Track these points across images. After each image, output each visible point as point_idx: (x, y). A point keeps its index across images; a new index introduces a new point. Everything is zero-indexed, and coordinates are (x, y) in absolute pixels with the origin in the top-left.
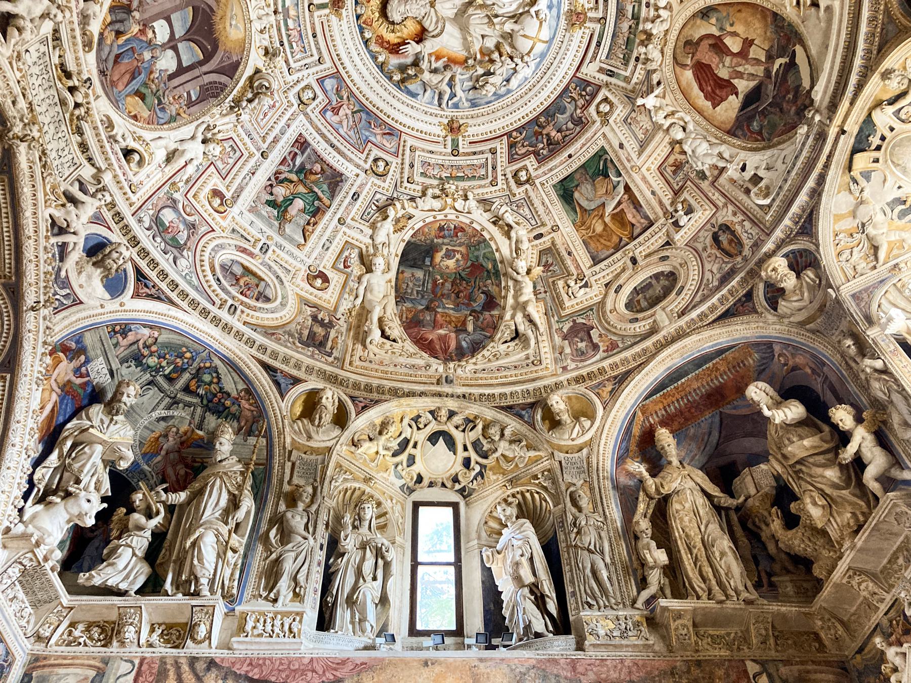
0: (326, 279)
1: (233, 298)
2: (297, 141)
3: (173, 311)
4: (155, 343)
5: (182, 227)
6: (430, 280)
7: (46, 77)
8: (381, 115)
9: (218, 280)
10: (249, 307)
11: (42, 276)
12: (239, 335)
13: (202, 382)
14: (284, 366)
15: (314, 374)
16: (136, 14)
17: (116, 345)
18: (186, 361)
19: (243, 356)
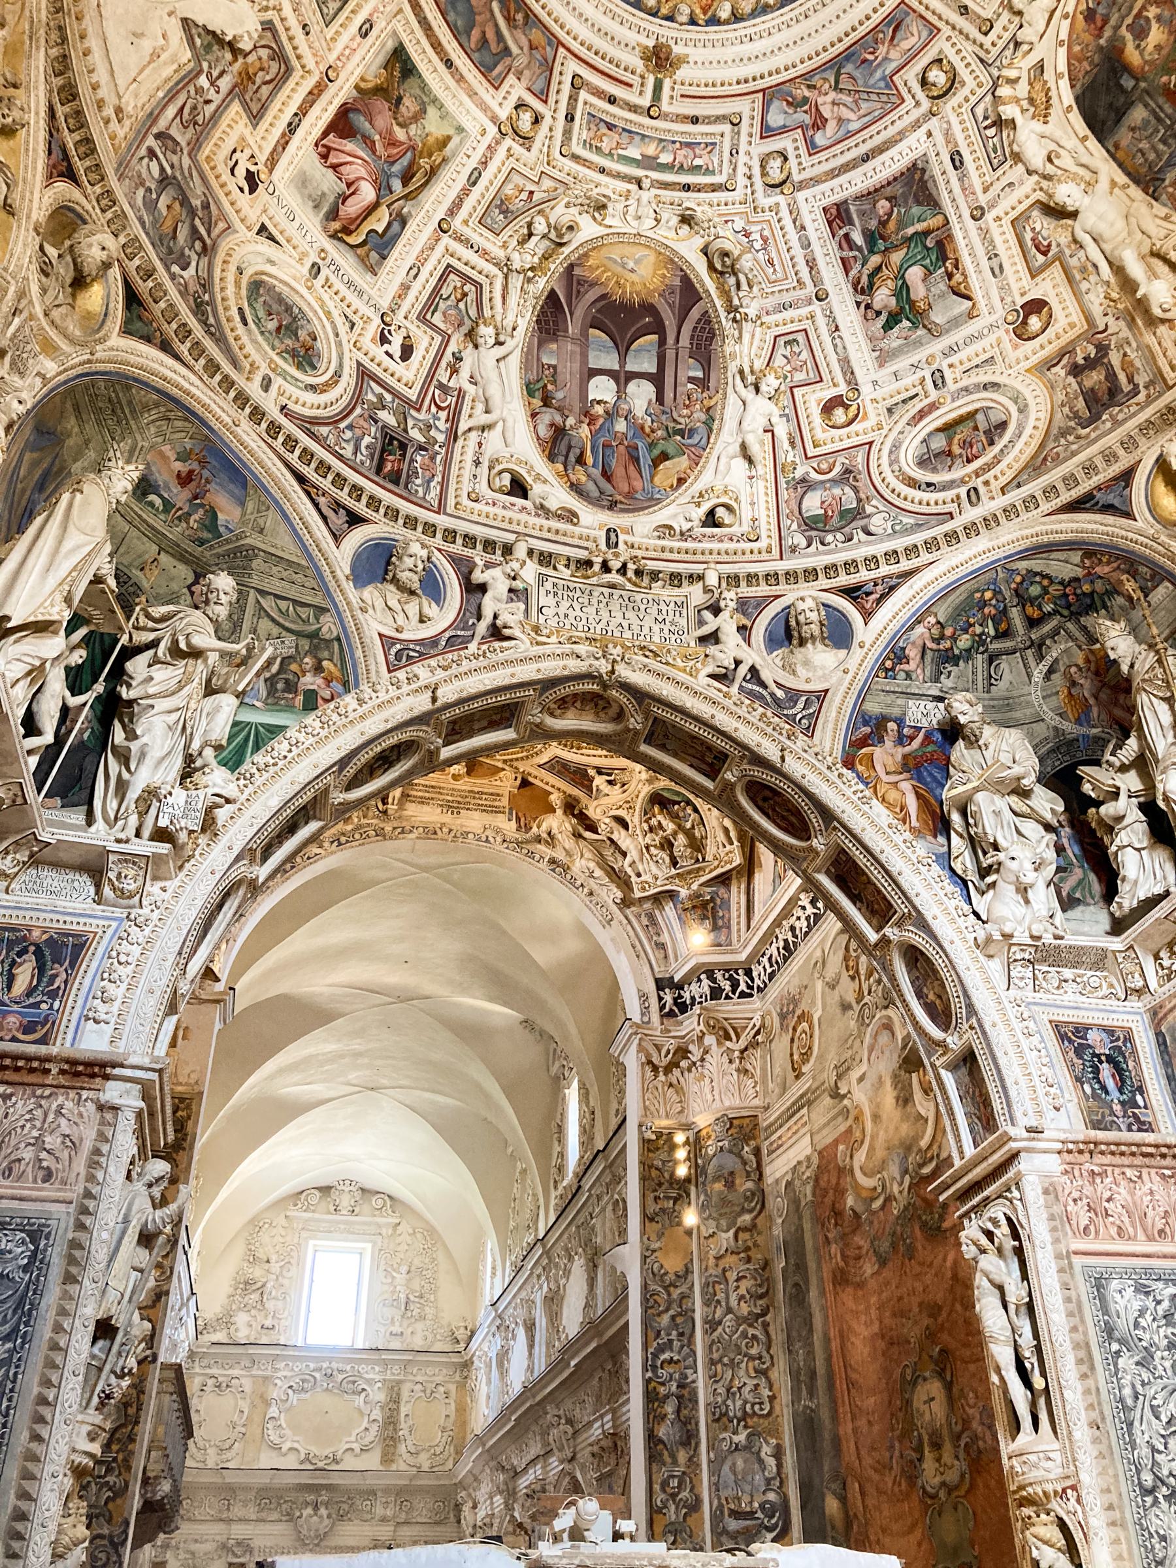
0: (1036, 306)
1: (963, 482)
2: (830, 223)
3: (917, 582)
4: (943, 627)
5: (837, 491)
6: (1161, 100)
7: (579, 593)
8: (862, 31)
9: (929, 485)
10: (988, 467)
11: (761, 724)
12: (1010, 512)
13: (1037, 598)
14: (1095, 479)
15: (1142, 441)
16: (571, 421)
17: (908, 675)
18: (994, 602)
19: (1037, 529)
